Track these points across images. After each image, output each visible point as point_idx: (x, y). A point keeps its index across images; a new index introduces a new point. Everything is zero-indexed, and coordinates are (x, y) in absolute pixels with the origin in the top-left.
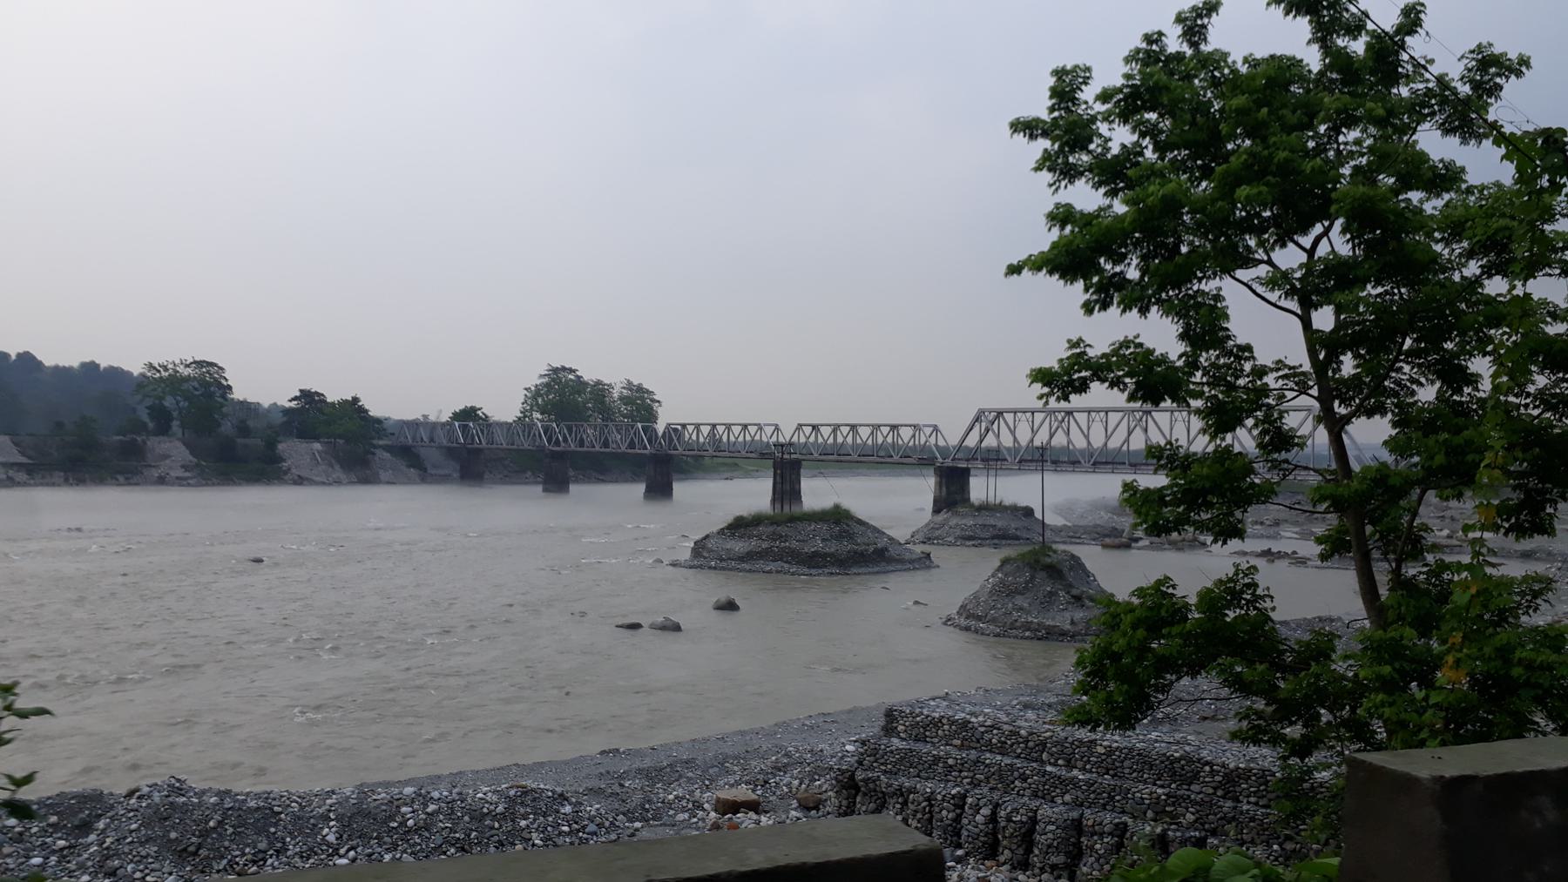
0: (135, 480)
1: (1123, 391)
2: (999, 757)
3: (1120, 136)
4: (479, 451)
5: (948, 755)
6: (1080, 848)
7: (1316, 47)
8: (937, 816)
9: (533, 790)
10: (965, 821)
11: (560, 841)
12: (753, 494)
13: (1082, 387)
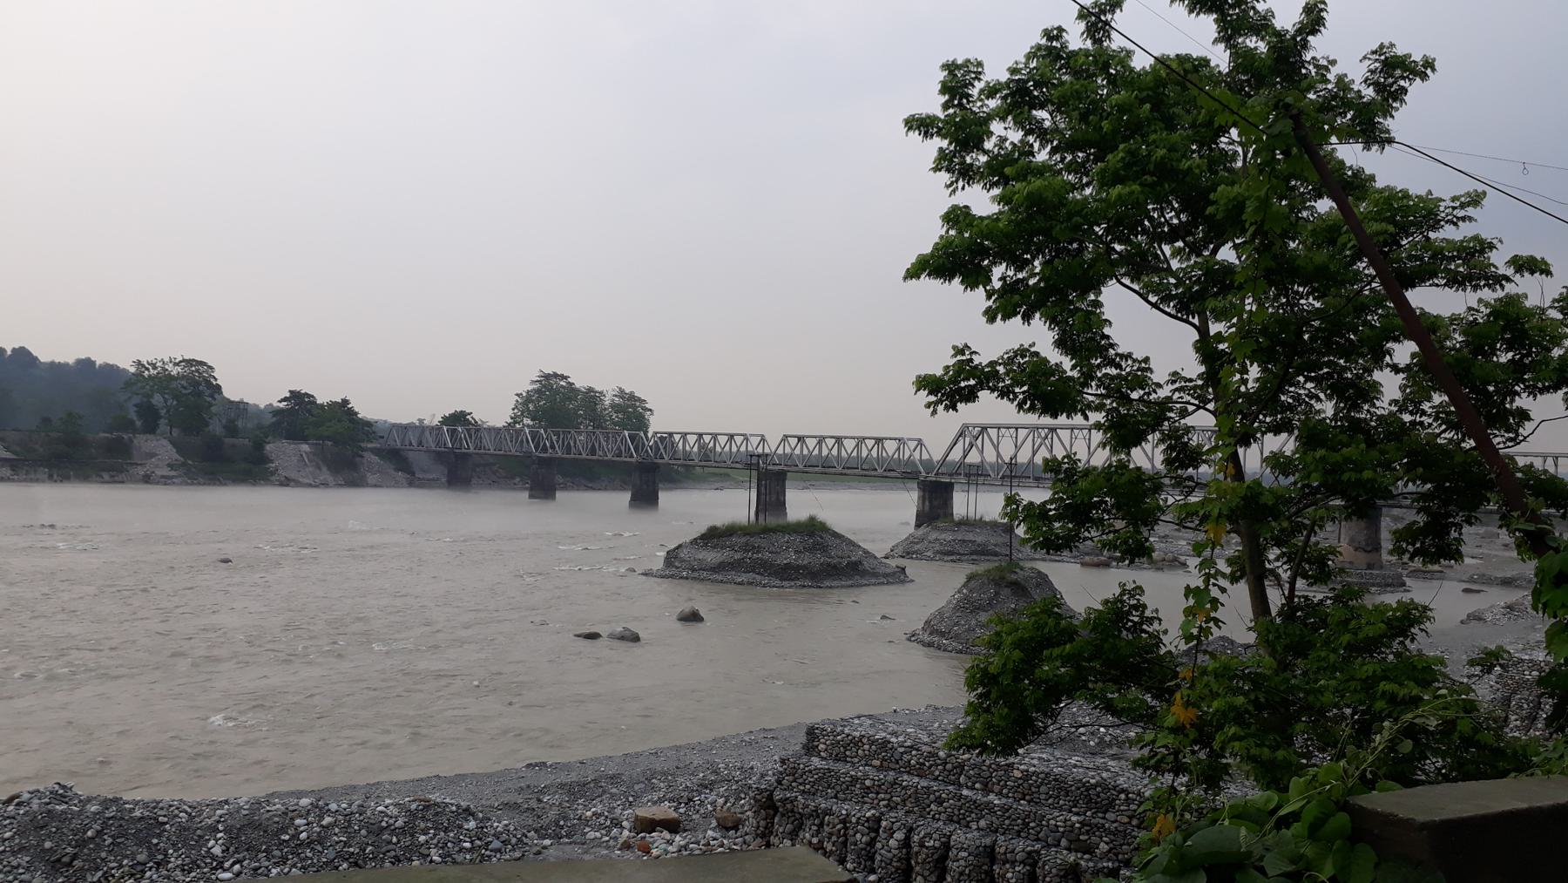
0: (120, 478)
1: (1012, 401)
2: (916, 780)
3: (1005, 133)
4: (466, 456)
5: (866, 777)
6: (993, 877)
7: (1222, 46)
8: (851, 840)
9: (437, 804)
10: (879, 845)
11: (459, 858)
12: (734, 505)
13: (970, 396)
